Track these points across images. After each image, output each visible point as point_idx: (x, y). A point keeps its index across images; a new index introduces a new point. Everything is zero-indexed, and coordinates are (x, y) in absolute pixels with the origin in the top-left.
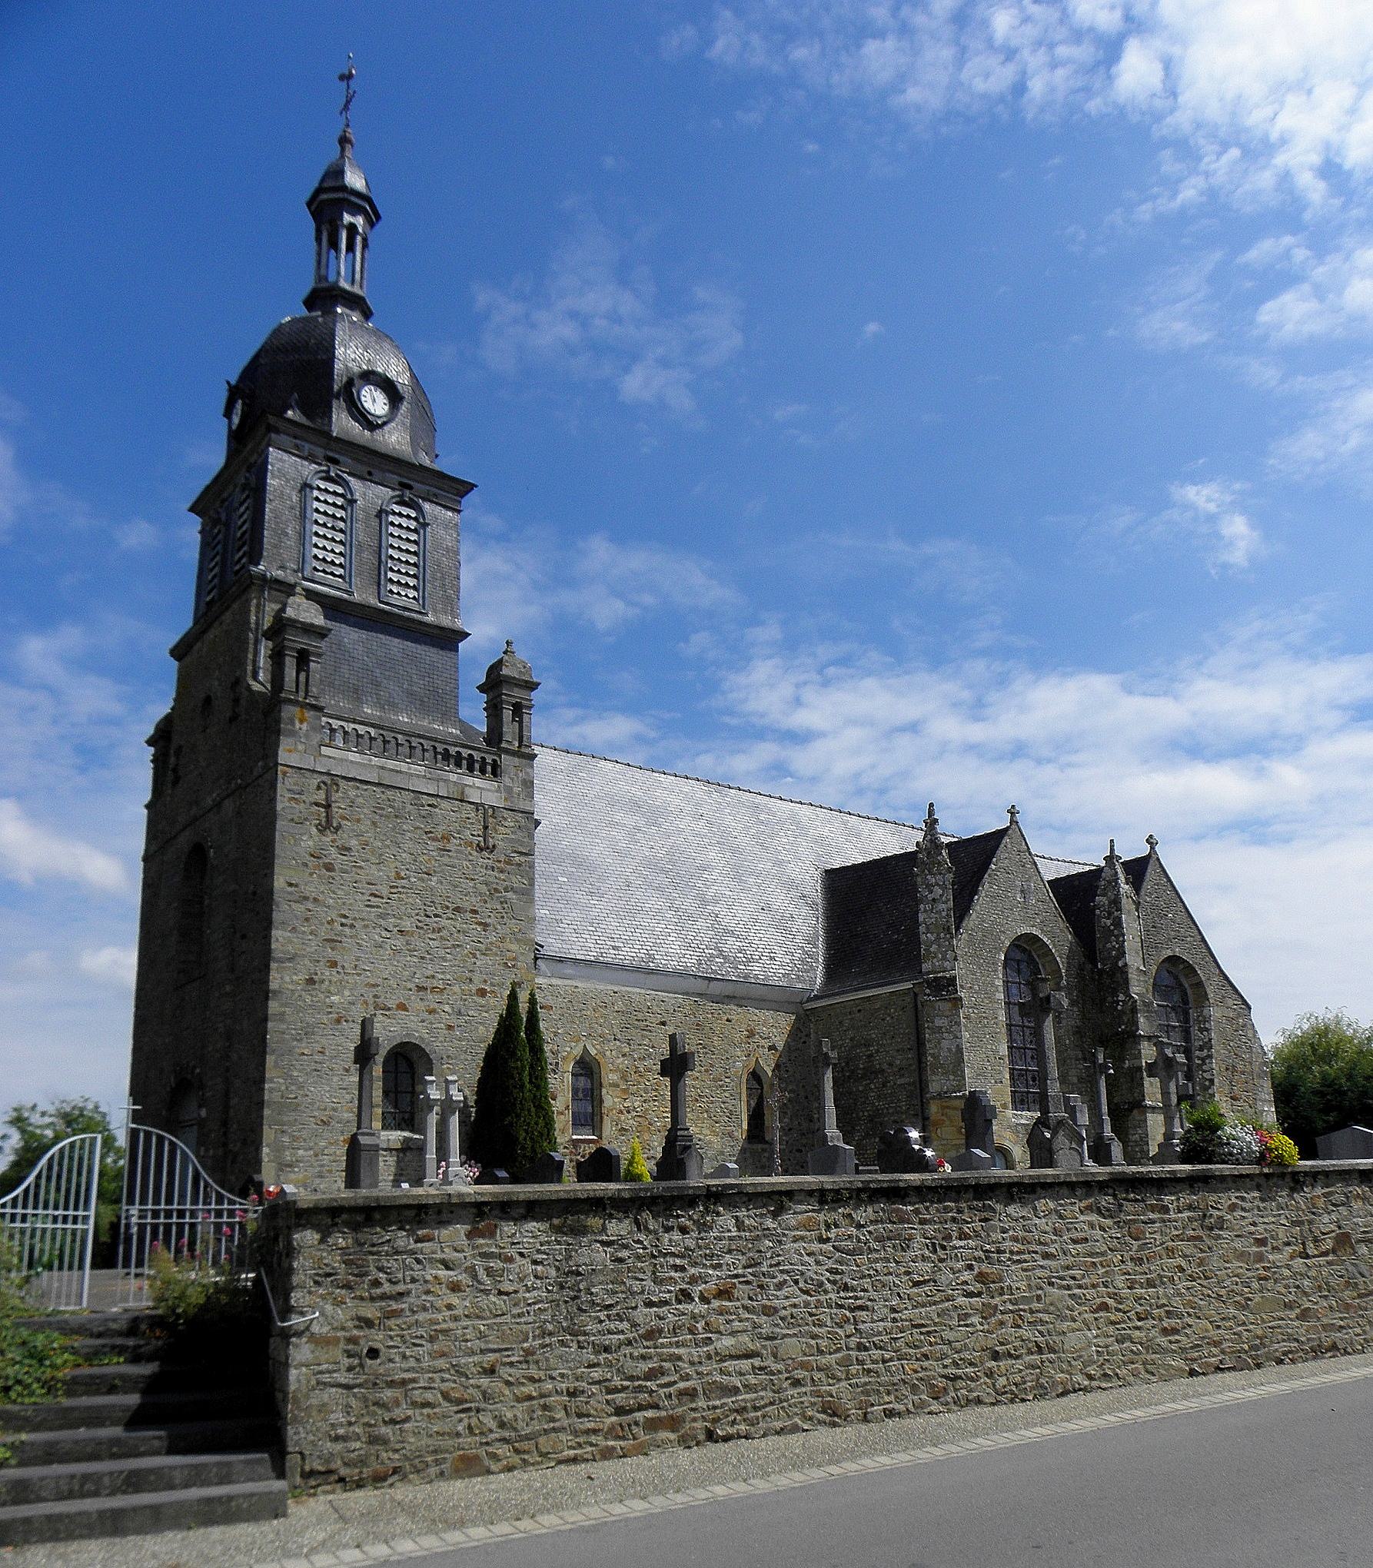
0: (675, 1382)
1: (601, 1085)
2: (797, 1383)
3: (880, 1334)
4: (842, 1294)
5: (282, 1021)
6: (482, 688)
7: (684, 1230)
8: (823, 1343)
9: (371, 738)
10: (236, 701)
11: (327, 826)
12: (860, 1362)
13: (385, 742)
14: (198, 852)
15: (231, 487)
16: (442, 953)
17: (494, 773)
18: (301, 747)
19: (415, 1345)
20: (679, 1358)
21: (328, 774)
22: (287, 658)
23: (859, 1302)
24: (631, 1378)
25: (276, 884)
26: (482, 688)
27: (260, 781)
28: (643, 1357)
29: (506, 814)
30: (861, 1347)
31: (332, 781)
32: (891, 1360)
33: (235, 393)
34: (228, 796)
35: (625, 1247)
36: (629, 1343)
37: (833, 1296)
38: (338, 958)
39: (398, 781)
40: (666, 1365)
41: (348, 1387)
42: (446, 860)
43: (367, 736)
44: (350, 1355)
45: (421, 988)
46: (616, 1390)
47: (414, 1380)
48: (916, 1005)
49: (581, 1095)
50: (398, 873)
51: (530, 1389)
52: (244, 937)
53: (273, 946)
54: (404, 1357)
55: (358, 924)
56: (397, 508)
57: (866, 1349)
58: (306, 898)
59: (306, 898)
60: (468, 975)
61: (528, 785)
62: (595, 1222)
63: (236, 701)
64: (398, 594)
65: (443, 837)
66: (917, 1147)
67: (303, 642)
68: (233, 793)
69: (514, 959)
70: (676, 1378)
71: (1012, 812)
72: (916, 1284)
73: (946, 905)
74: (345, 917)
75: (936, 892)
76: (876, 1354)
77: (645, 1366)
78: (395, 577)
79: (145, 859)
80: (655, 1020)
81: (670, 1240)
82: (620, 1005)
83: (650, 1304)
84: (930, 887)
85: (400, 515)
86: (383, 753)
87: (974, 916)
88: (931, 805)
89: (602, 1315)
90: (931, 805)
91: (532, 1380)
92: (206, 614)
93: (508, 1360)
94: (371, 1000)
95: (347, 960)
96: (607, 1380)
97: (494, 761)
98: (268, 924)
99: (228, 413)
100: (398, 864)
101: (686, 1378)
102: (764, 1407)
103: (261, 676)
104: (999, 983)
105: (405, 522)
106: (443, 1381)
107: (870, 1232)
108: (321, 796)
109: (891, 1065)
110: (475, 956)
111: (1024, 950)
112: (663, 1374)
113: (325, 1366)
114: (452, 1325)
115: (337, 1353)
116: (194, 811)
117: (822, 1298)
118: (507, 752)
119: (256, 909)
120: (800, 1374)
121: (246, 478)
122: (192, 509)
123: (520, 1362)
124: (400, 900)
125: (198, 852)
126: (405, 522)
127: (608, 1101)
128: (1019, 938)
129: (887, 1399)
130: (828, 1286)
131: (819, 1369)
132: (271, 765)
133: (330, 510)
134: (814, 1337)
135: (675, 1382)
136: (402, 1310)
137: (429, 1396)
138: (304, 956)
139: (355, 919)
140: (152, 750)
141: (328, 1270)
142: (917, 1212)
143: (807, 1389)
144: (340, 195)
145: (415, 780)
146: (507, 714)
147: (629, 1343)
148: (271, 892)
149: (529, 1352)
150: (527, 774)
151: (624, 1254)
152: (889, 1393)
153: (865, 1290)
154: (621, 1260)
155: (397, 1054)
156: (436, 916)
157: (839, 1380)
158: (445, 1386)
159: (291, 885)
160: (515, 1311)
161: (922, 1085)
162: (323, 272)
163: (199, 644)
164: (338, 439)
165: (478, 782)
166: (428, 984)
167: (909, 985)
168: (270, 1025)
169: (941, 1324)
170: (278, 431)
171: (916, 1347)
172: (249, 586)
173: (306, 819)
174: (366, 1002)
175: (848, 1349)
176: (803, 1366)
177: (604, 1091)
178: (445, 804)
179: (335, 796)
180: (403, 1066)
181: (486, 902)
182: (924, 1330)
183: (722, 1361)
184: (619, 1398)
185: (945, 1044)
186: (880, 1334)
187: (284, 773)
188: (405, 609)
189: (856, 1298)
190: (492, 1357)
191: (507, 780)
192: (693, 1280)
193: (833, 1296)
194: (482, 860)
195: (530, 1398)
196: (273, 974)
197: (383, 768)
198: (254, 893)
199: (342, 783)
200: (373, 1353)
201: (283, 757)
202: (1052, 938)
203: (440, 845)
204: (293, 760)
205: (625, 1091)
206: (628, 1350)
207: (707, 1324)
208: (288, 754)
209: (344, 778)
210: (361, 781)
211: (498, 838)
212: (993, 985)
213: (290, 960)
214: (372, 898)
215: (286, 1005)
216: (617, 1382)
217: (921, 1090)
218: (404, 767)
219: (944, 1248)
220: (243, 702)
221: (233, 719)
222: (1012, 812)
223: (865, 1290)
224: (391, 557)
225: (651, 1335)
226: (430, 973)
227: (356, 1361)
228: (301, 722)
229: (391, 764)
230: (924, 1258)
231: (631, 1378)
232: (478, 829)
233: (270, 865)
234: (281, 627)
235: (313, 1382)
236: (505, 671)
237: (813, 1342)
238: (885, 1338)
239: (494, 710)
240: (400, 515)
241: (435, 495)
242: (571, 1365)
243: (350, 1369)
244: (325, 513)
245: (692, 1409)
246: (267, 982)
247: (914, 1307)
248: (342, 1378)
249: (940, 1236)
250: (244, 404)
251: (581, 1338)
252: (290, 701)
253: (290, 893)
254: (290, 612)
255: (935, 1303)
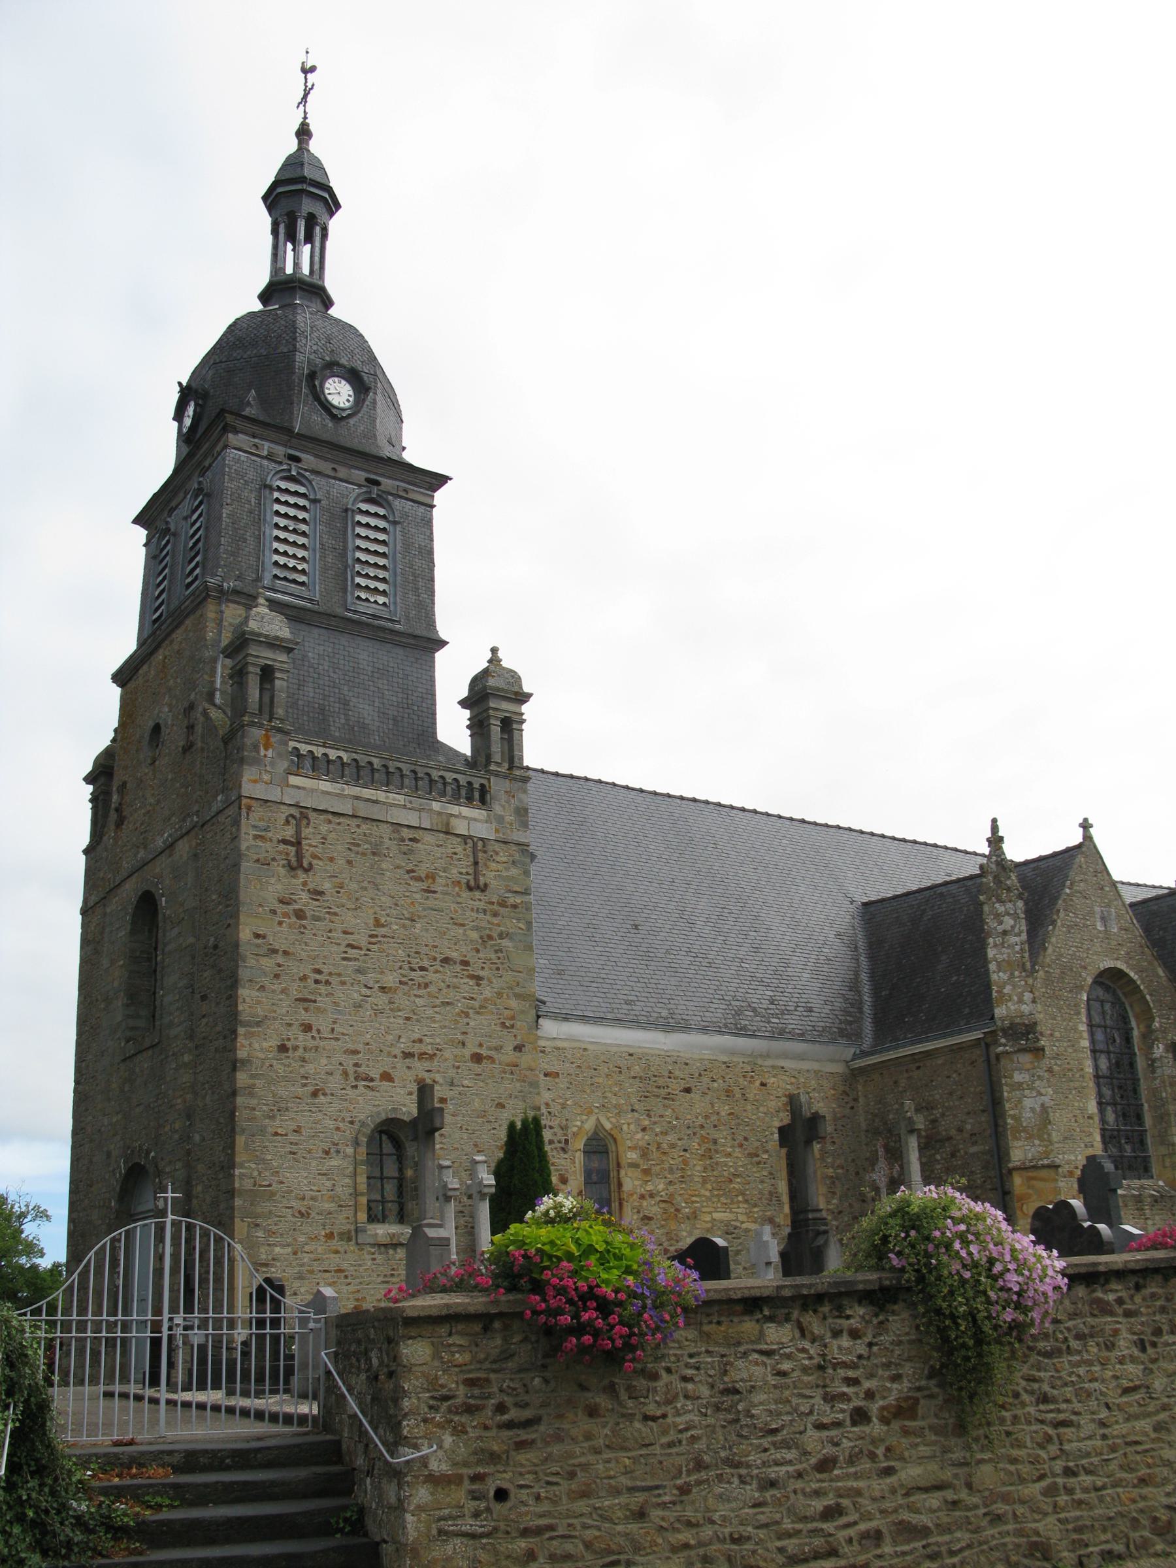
0: (855, 1523)
1: (619, 1165)
2: (997, 1519)
3: (1088, 1455)
4: (1042, 1407)
5: (251, 1095)
6: (464, 703)
7: (855, 1334)
8: (1025, 1469)
9: (343, 764)
10: (191, 728)
11: (298, 865)
12: (1069, 1491)
13: (358, 768)
14: (147, 903)
15: (181, 495)
16: (430, 1012)
17: (483, 801)
18: (266, 777)
19: (549, 1483)
20: (858, 1493)
21: (297, 806)
22: (251, 676)
23: (1062, 1416)
24: (805, 1519)
25: (241, 935)
26: (464, 703)
27: (221, 818)
28: (817, 1493)
29: (497, 847)
30: (1069, 1472)
31: (302, 815)
32: (1104, 1487)
33: (187, 393)
34: (182, 837)
35: (789, 1357)
36: (800, 1475)
37: (1031, 1410)
38: (312, 1020)
39: (375, 812)
40: (845, 1502)
41: (473, 1536)
42: (431, 903)
43: (338, 763)
44: (475, 1496)
45: (407, 1055)
46: (789, 1535)
47: (551, 1528)
48: (988, 1060)
49: (594, 1178)
50: (377, 920)
51: (686, 1536)
52: (204, 998)
53: (240, 1008)
54: (538, 1498)
55: (335, 980)
56: (364, 507)
57: (1075, 1474)
58: (275, 951)
59: (275, 951)
60: (461, 1037)
61: (522, 813)
62: (748, 1326)
63: (191, 728)
64: (367, 600)
65: (427, 877)
66: (1086, 1224)
67: (267, 656)
68: (187, 833)
69: (513, 1018)
70: (856, 1517)
71: (1086, 825)
72: (1127, 1391)
73: (1018, 939)
74: (319, 972)
75: (1006, 922)
76: (1087, 1480)
77: (818, 1505)
78: (363, 582)
79: (84, 912)
80: (676, 1087)
81: (839, 1347)
82: (637, 1070)
83: (820, 1427)
84: (998, 916)
85: (367, 513)
86: (357, 780)
87: (1050, 951)
88: (994, 821)
89: (766, 1442)
90: (994, 821)
91: (689, 1524)
92: (154, 633)
93: (659, 1500)
94: (351, 1070)
95: (322, 1023)
96: (777, 1523)
97: (482, 786)
98: (233, 982)
99: (179, 416)
100: (378, 909)
101: (868, 1517)
102: (961, 1550)
103: (218, 699)
104: (1083, 1028)
105: (373, 522)
106: (585, 1527)
107: (1068, 1329)
108: (289, 832)
109: (960, 1130)
110: (467, 1015)
111: (1107, 989)
112: (841, 1514)
113: (447, 1511)
114: (591, 1458)
115: (460, 1495)
116: (142, 854)
117: (1019, 1412)
118: (497, 774)
119: (220, 966)
120: (1000, 1508)
121: (200, 483)
122: (138, 520)
123: (674, 1503)
124: (382, 951)
125: (147, 903)
126: (373, 522)
127: (628, 1185)
128: (1102, 974)
129: (1103, 1537)
130: (1025, 1397)
131: (1022, 1502)
132: (236, 802)
133: (292, 512)
134: (1014, 1461)
135: (855, 1523)
136: (533, 1441)
137: (569, 1547)
138: (275, 1019)
139: (330, 974)
140: (90, 788)
141: (444, 1392)
142: (1120, 1301)
143: (1010, 1527)
144: (299, 187)
145: (394, 810)
146: (495, 730)
147: (800, 1475)
148: (237, 945)
149: (684, 1490)
150: (520, 801)
151: (786, 1366)
152: (1104, 1530)
153: (1067, 1401)
154: (783, 1374)
155: (381, 1132)
156: (422, 969)
157: (1046, 1514)
158: (589, 1534)
159: (257, 936)
160: (664, 1440)
161: (1000, 1153)
162: (279, 265)
163: (145, 667)
164: (300, 436)
165: (465, 811)
166: (416, 1049)
167: (977, 1035)
168: (240, 1100)
169: (1159, 1440)
170: (236, 431)
171: (1132, 1470)
172: (205, 599)
173: (274, 859)
174: (345, 1073)
175: (1054, 1475)
176: (1006, 1498)
177: (623, 1173)
178: (428, 838)
179: (306, 832)
180: (388, 1147)
181: (478, 951)
182: (1139, 1448)
183: (907, 1495)
184: (791, 1545)
185: (1028, 1103)
186: (1088, 1455)
187: (249, 808)
188: (375, 617)
189: (1059, 1411)
190: (640, 1497)
191: (497, 808)
192: (870, 1395)
193: (1031, 1410)
194: (478, 900)
195: (686, 1546)
196: (241, 1040)
197: (357, 798)
198: (216, 947)
199: (312, 815)
200: (501, 1495)
201: (248, 789)
202: (1140, 971)
203: (424, 885)
204: (259, 791)
205: (646, 1172)
206: (799, 1484)
207: (888, 1449)
208: (253, 783)
209: (315, 810)
210: (333, 813)
211: (489, 876)
212: (1075, 1029)
213: (258, 1024)
214: (349, 950)
215: (253, 1076)
216: (788, 1525)
217: (1000, 1159)
218: (381, 796)
219: (1154, 1345)
220: (199, 729)
221: (187, 748)
222: (1086, 825)
223: (1067, 1401)
224: (358, 560)
225: (825, 1465)
226: (417, 1036)
227: (483, 1505)
228: (266, 749)
229: (367, 793)
230: (1133, 1360)
231: (805, 1519)
232: (465, 866)
233: (235, 915)
234: (241, 643)
235: (434, 1532)
236: (491, 682)
237: (1012, 1468)
238: (1095, 1460)
239: (478, 727)
240: (367, 513)
241: (405, 491)
242: (734, 1505)
243: (476, 1515)
244: (286, 516)
245: (880, 1557)
246: (234, 1050)
247: (1127, 1420)
248: (469, 1525)
249: (1149, 1331)
250: (196, 405)
251: (743, 1471)
252: (253, 724)
253: (258, 946)
254: (253, 625)
255: (1149, 1415)
